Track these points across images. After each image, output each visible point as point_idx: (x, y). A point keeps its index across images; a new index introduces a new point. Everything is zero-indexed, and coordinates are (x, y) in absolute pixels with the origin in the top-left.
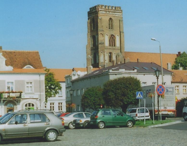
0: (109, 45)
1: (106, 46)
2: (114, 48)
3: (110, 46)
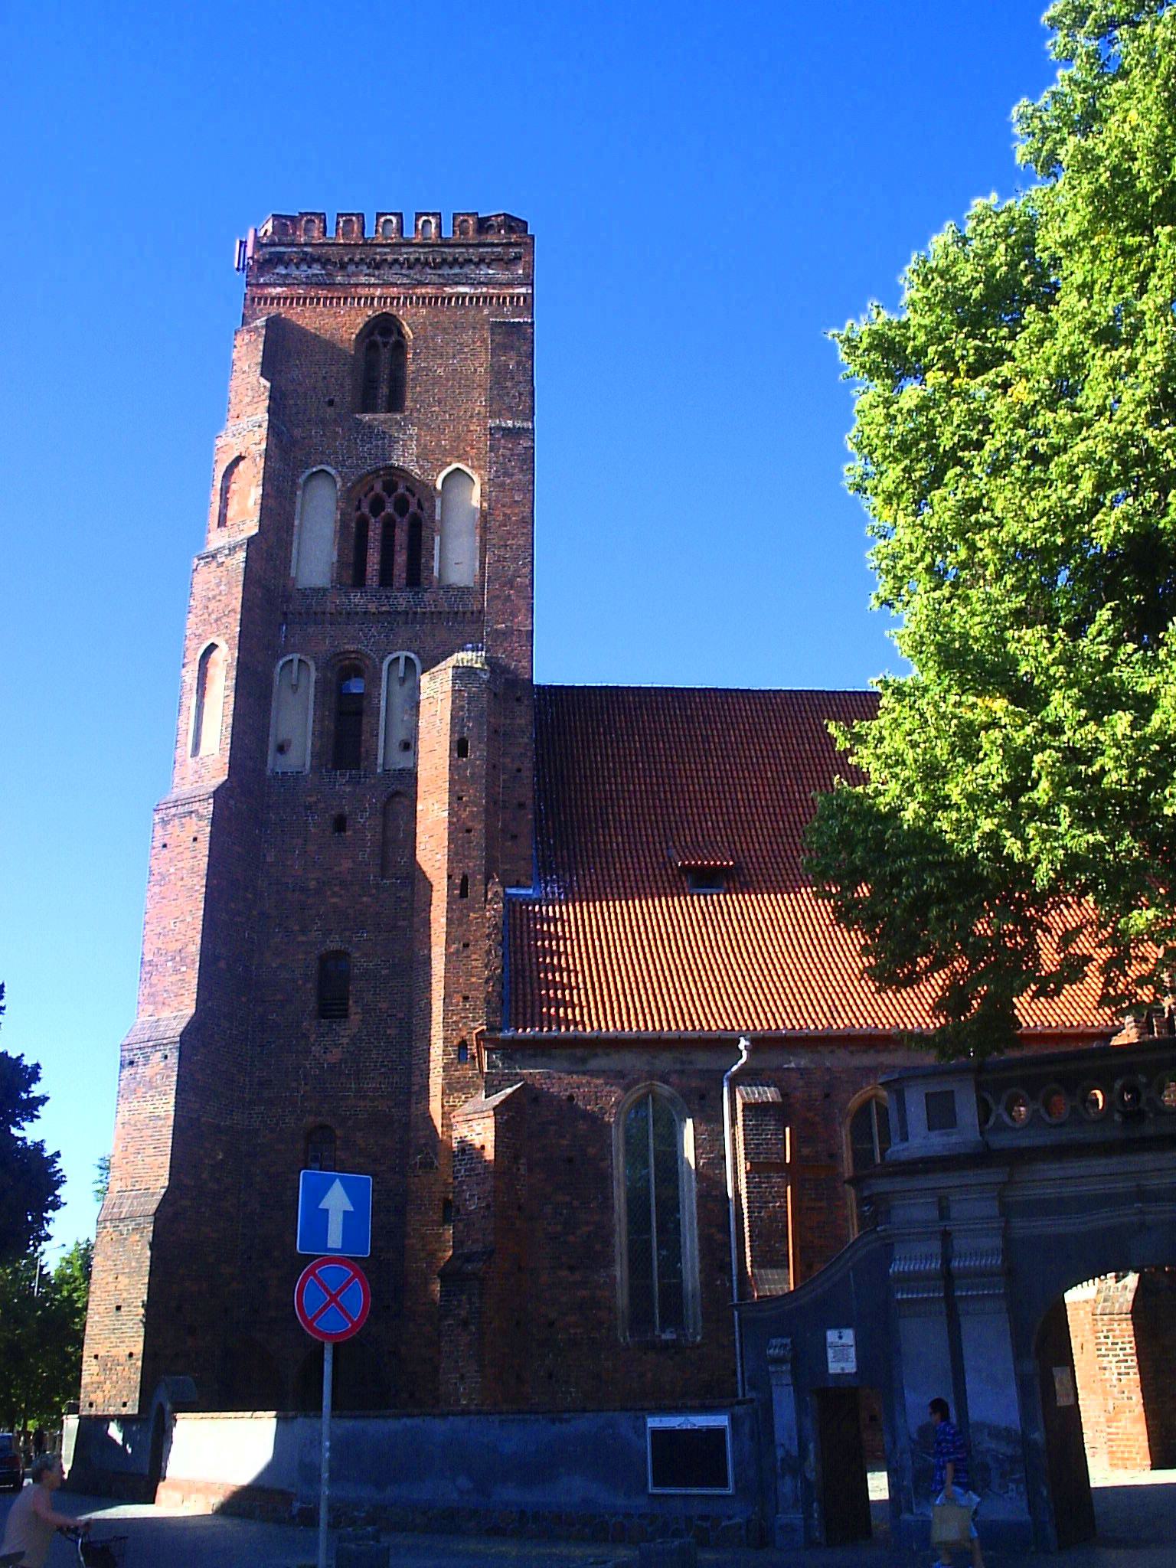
0: (348, 575)
1: (305, 593)
2: (402, 600)
3: (359, 580)
